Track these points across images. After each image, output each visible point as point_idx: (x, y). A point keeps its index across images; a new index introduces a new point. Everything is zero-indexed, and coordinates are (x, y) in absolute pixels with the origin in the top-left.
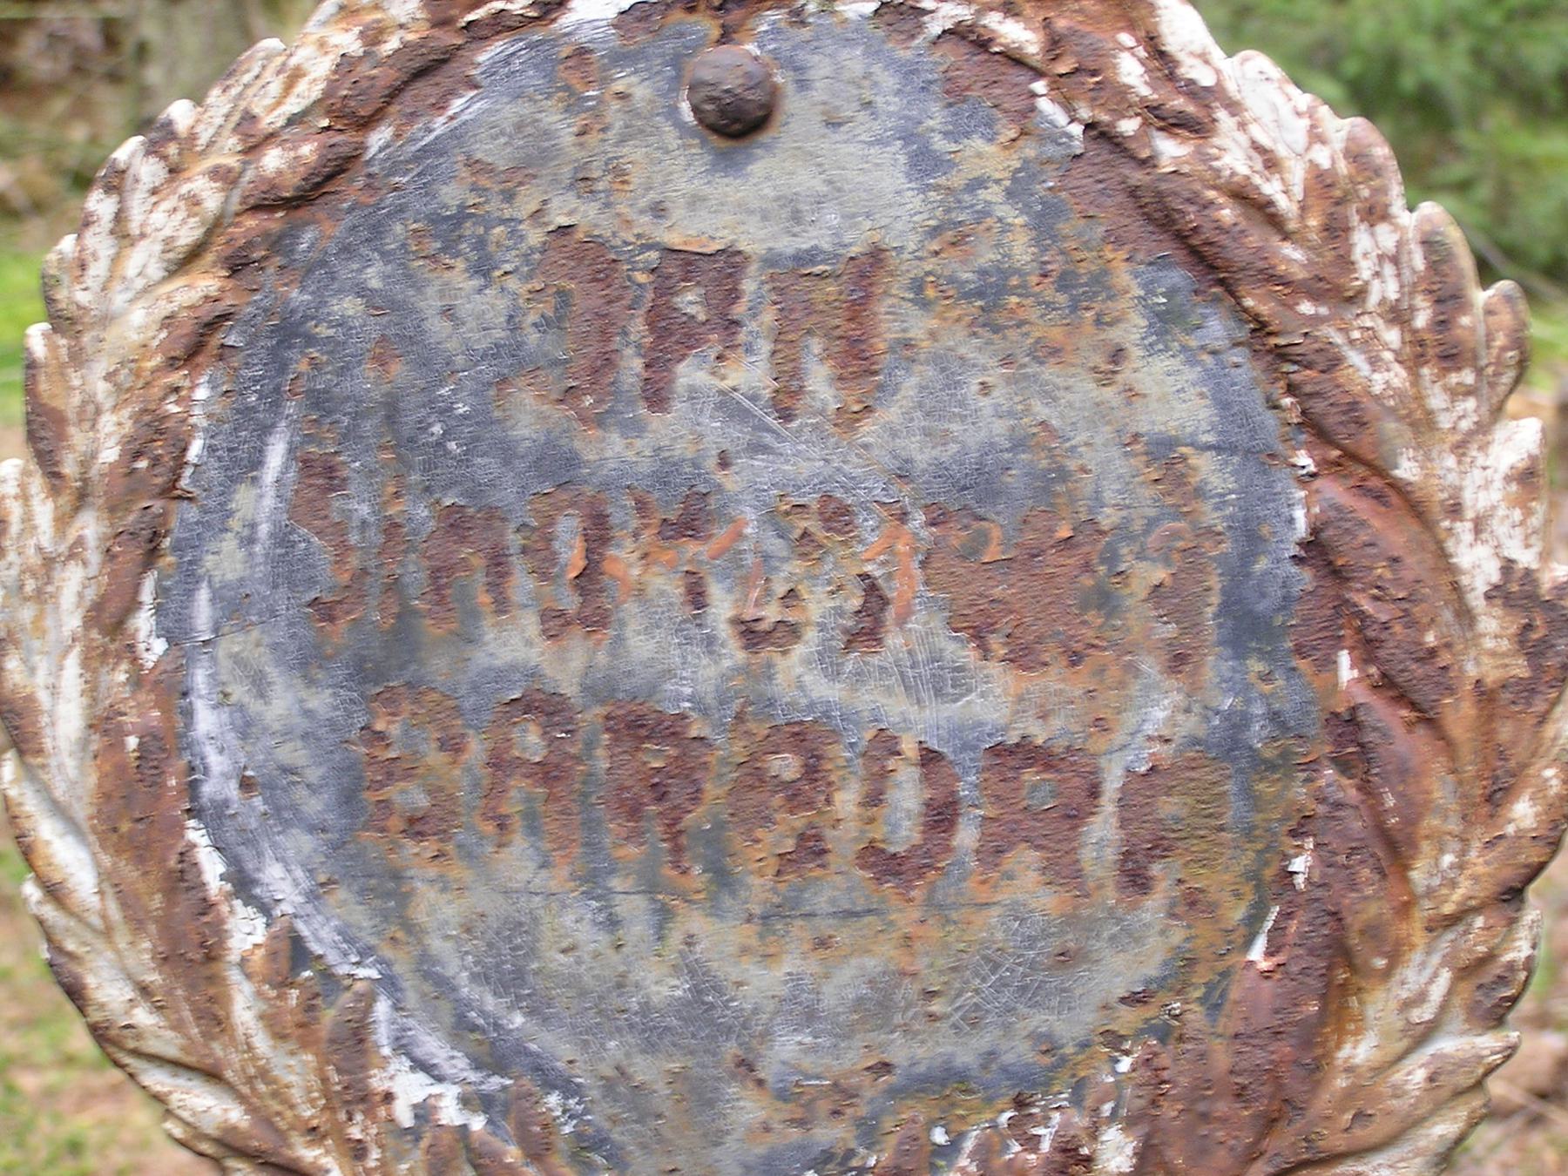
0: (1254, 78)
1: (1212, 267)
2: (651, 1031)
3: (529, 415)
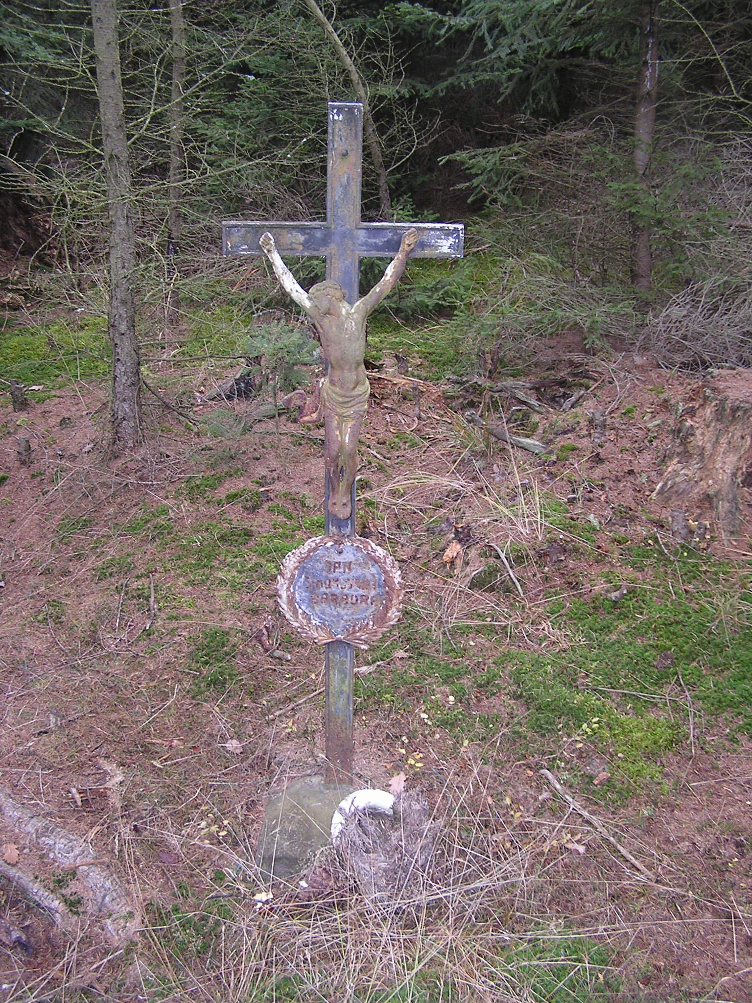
1: (376, 562)
3: (324, 573)
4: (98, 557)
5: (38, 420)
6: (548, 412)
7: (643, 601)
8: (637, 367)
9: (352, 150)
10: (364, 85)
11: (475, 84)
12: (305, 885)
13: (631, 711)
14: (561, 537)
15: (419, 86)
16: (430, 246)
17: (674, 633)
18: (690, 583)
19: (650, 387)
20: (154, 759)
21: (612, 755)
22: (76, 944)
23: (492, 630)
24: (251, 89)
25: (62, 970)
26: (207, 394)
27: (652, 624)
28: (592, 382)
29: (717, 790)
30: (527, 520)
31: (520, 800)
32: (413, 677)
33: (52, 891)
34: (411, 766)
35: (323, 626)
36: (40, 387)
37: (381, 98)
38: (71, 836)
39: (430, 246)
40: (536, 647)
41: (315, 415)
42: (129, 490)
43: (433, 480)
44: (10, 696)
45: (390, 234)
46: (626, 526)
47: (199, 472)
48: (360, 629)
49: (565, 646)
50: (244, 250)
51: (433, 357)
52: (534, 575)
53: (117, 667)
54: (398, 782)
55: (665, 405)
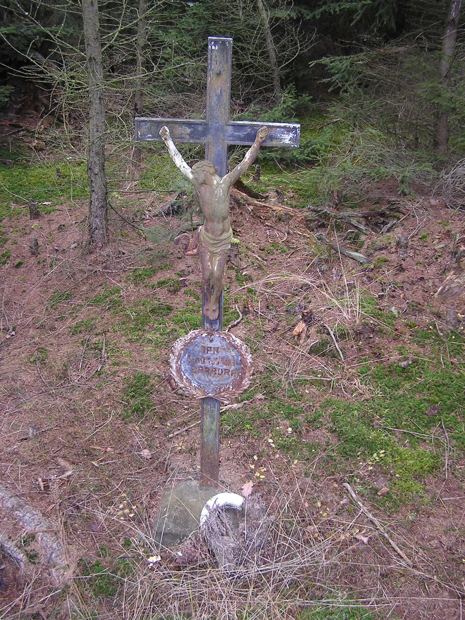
0: (237, 339)
1: (235, 348)
2: (207, 382)
3: (201, 354)
4: (74, 319)
5: (44, 226)
6: (371, 234)
7: (422, 369)
8: (432, 207)
9: (224, 70)
10: (266, 10)
11: (340, 10)
12: (181, 555)
13: (408, 445)
14: (372, 322)
15: (304, 12)
16: (276, 139)
17: (441, 392)
18: (455, 357)
19: (439, 221)
20: (94, 460)
21: (392, 475)
22: (31, 584)
23: (321, 383)
24: (194, 11)
25: (21, 600)
26: (152, 213)
27: (427, 385)
28: (401, 215)
29: (460, 504)
30: (349, 309)
31: (328, 503)
32: (266, 413)
33: (19, 548)
34: (258, 478)
35: (199, 388)
36: (50, 203)
37: (277, 19)
38: (34, 512)
39: (276, 139)
40: (349, 396)
41: (195, 251)
42: (97, 275)
43: (294, 277)
44: (7, 412)
45: (249, 130)
46: (415, 315)
47: (142, 266)
48: (224, 391)
49: (368, 397)
50: (149, 137)
51: (301, 192)
52: (352, 347)
53: (77, 395)
54: (248, 488)
55: (448, 234)
